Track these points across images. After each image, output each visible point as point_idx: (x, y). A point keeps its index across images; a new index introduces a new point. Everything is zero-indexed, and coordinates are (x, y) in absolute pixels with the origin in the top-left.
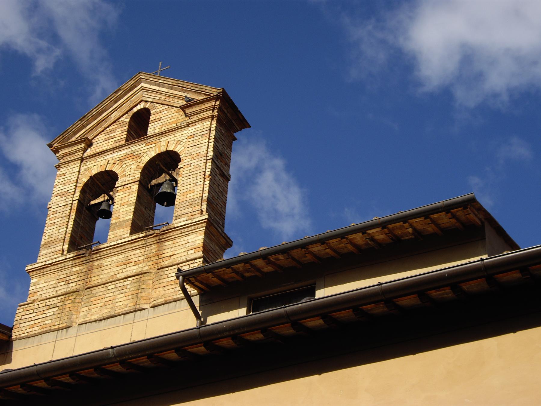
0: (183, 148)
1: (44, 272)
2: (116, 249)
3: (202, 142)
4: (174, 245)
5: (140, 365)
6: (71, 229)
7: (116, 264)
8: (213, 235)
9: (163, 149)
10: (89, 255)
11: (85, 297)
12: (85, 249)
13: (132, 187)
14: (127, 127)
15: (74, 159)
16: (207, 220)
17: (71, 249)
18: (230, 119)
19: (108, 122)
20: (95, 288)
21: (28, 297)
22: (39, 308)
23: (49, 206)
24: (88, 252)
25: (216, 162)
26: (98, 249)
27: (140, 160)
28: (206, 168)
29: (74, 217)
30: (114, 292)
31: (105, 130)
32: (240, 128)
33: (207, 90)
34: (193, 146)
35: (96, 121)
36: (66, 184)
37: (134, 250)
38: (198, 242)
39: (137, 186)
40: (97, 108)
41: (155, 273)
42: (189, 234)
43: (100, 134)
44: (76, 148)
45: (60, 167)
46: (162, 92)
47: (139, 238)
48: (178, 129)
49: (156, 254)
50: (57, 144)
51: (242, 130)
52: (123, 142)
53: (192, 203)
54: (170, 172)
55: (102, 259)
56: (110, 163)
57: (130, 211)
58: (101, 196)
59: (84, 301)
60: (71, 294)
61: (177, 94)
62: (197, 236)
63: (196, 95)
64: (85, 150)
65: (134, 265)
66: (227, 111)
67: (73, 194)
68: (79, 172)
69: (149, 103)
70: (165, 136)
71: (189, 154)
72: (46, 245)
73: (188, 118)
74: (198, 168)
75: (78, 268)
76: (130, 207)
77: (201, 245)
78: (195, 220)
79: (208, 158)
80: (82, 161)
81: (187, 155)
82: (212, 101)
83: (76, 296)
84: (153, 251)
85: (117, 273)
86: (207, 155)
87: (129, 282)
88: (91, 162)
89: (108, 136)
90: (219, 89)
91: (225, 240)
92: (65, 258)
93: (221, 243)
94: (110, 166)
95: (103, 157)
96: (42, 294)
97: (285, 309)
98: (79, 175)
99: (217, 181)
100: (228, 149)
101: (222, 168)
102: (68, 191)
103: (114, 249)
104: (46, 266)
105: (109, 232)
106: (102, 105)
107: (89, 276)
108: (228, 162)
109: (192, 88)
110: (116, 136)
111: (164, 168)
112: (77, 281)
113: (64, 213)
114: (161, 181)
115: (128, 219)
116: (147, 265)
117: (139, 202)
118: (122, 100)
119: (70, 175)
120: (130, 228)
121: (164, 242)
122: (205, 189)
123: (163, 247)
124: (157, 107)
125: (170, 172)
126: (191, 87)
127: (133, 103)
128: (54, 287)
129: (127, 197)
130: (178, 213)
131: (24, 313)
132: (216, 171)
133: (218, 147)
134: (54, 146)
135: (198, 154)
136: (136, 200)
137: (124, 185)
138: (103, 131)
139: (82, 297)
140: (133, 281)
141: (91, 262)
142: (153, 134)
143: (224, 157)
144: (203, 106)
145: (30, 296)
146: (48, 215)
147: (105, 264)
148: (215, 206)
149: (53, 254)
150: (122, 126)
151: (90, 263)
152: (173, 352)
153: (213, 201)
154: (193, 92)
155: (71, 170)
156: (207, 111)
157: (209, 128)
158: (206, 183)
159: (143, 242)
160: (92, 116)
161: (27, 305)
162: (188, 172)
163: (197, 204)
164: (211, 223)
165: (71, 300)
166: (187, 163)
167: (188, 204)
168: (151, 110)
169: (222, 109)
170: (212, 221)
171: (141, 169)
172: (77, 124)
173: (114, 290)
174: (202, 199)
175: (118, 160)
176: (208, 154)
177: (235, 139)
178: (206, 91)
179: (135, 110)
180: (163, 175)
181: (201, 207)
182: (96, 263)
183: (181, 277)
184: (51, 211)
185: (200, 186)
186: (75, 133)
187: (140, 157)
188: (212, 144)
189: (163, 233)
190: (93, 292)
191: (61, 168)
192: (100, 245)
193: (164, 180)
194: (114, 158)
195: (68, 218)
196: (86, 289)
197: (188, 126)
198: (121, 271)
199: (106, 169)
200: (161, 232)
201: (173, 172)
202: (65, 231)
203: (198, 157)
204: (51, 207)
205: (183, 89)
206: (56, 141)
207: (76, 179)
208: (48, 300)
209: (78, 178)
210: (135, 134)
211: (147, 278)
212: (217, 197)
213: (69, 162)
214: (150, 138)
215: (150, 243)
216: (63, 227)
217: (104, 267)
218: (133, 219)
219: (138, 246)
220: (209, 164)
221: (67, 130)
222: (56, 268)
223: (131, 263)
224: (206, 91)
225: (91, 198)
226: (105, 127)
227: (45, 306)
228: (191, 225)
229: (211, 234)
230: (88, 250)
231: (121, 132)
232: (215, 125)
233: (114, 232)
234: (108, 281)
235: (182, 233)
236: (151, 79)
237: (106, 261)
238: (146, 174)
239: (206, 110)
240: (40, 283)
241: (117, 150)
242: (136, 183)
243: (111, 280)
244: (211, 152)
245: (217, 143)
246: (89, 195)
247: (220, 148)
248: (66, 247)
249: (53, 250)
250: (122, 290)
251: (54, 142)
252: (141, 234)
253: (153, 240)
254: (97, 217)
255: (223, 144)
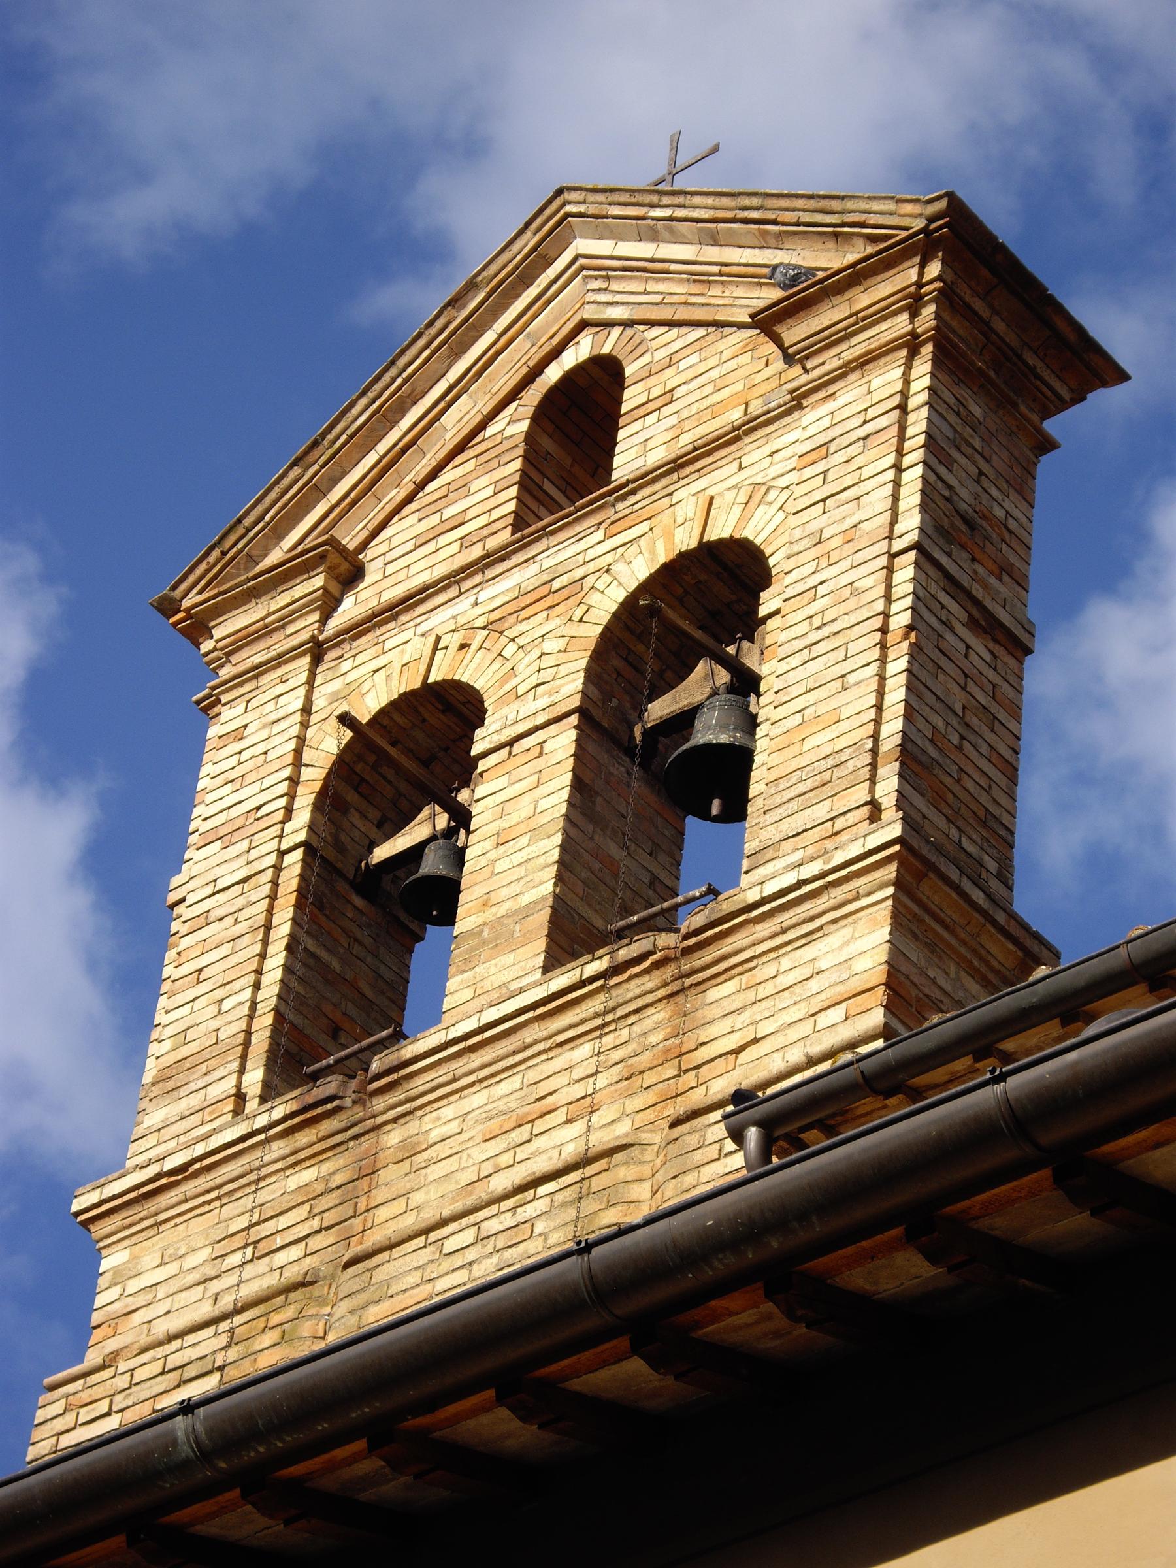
0: (781, 515)
1: (156, 1214)
2: (482, 1052)
3: (866, 473)
4: (751, 995)
5: (364, 1496)
6: (276, 989)
7: (481, 1127)
8: (946, 927)
9: (686, 540)
10: (354, 1102)
11: (342, 1303)
12: (335, 1077)
13: (548, 747)
14: (517, 464)
15: (280, 656)
16: (897, 848)
17: (276, 1081)
18: (1012, 349)
19: (432, 453)
20: (385, 1256)
21: (90, 1344)
22: (134, 1389)
23: (172, 897)
24: (353, 1084)
25: (944, 560)
26: (396, 1063)
27: (583, 608)
28: (888, 598)
29: (286, 929)
30: (471, 1263)
31: (420, 495)
32: (1071, 390)
33: (876, 213)
34: (824, 500)
35: (372, 458)
36: (248, 780)
37: (567, 1047)
38: (861, 965)
39: (573, 734)
40: (371, 395)
41: (663, 1145)
42: (820, 928)
43: (396, 519)
44: (288, 600)
45: (218, 701)
46: (673, 267)
47: (582, 984)
48: (754, 429)
49: (667, 1051)
50: (200, 593)
51: (1083, 399)
52: (505, 536)
53: (826, 776)
54: (731, 650)
55: (419, 1113)
56: (446, 648)
57: (542, 860)
58: (420, 816)
59: (337, 1324)
60: (280, 1300)
61: (743, 261)
62: (856, 935)
63: (828, 250)
64: (329, 604)
65: (569, 1121)
66: (991, 306)
67: (283, 822)
68: (307, 710)
69: (616, 331)
70: (696, 475)
71: (807, 540)
72: (162, 1084)
73: (797, 370)
74: (852, 604)
75: (311, 1169)
76: (541, 844)
77: (879, 975)
78: (839, 858)
79: (898, 545)
80: (317, 660)
81: (796, 548)
82: (906, 264)
83: (299, 1306)
84: (653, 1039)
85: (487, 1168)
86: (891, 530)
87: (541, 1205)
88: (360, 659)
89: (435, 519)
90: (930, 202)
91: (1011, 946)
92: (245, 1132)
93: (995, 963)
94: (447, 661)
95: (412, 624)
96: (149, 1322)
97: (998, 1088)
98: (305, 725)
99: (959, 658)
100: (1014, 496)
101: (977, 591)
102: (258, 808)
103: (473, 1056)
104: (164, 1181)
105: (448, 980)
106: (393, 372)
107: (362, 1206)
108: (1013, 559)
109: (807, 218)
110: (471, 514)
111: (698, 634)
112: (308, 1236)
113: (242, 916)
114: (690, 700)
115: (535, 902)
116: (628, 1111)
117: (584, 814)
118: (489, 337)
119: (264, 734)
120: (541, 944)
121: (702, 987)
122: (889, 699)
123: (699, 1014)
124: (655, 344)
125: (731, 650)
126: (801, 213)
127: (543, 340)
128: (205, 1281)
129: (527, 798)
130: (764, 835)
131: (69, 1419)
132: (943, 607)
133: (950, 487)
134: (186, 603)
135: (850, 535)
136: (570, 802)
137: (511, 743)
138: (409, 499)
139: (327, 1310)
140: (559, 1197)
141: (367, 1137)
142: (638, 473)
143: (987, 538)
144: (864, 298)
145: (97, 1335)
146: (172, 940)
147: (434, 1135)
148: (947, 780)
149: (196, 1119)
150: (496, 460)
151: (363, 1139)
152: (484, 1409)
153: (933, 752)
154: (815, 237)
155: (270, 706)
156: (885, 318)
157: (896, 400)
158: (891, 669)
159: (596, 1004)
160: (351, 437)
161: (82, 1381)
162: (804, 627)
163: (851, 777)
164: (924, 860)
165: (279, 1329)
166: (800, 588)
167: (809, 784)
168: (624, 363)
169: (961, 298)
170: (925, 851)
171: (589, 653)
172: (285, 482)
173: (471, 1255)
174: (874, 751)
175: (484, 628)
176: (897, 526)
177: (1047, 445)
178: (873, 219)
179: (553, 373)
180: (702, 668)
181: (872, 791)
182: (393, 1137)
183: (753, 1134)
184: (183, 919)
185: (863, 689)
186: (279, 532)
187: (582, 594)
188: (913, 478)
189: (693, 941)
190: (380, 1275)
191: (224, 705)
192: (405, 1042)
193: (707, 691)
194: (462, 620)
195: (260, 937)
196: (347, 1265)
197: (799, 407)
198: (506, 1159)
199: (431, 680)
200: (686, 937)
201: (746, 644)
202: (248, 1004)
203: (849, 548)
204: (183, 900)
205: (767, 232)
206: (192, 578)
207: (292, 745)
208: (176, 1344)
209: (301, 740)
210: (564, 493)
211: (622, 1173)
212: (962, 738)
213: (258, 671)
214: (623, 498)
215: (640, 1003)
216: (237, 985)
217: (429, 1151)
218: (556, 897)
219: (583, 1022)
220: (905, 573)
221: (239, 521)
222: (212, 1184)
223: (555, 1110)
224: (872, 222)
225: (374, 833)
226: (419, 479)
227: (162, 1373)
228: (827, 882)
229: (927, 918)
230: (353, 1077)
231: (490, 491)
232: (926, 381)
233: (470, 973)
234: (446, 1213)
235: (784, 931)
236: (616, 211)
237: (439, 1119)
238: (619, 674)
239: (882, 315)
240: (139, 1267)
241: (478, 579)
242: (565, 721)
243: (458, 1206)
244: (912, 516)
245: (942, 470)
246: (363, 816)
247: (964, 493)
248: (254, 1078)
249: (195, 1101)
250: (510, 1250)
251: (183, 586)
252: (591, 961)
253: (650, 985)
254: (414, 926)
255: (981, 473)
